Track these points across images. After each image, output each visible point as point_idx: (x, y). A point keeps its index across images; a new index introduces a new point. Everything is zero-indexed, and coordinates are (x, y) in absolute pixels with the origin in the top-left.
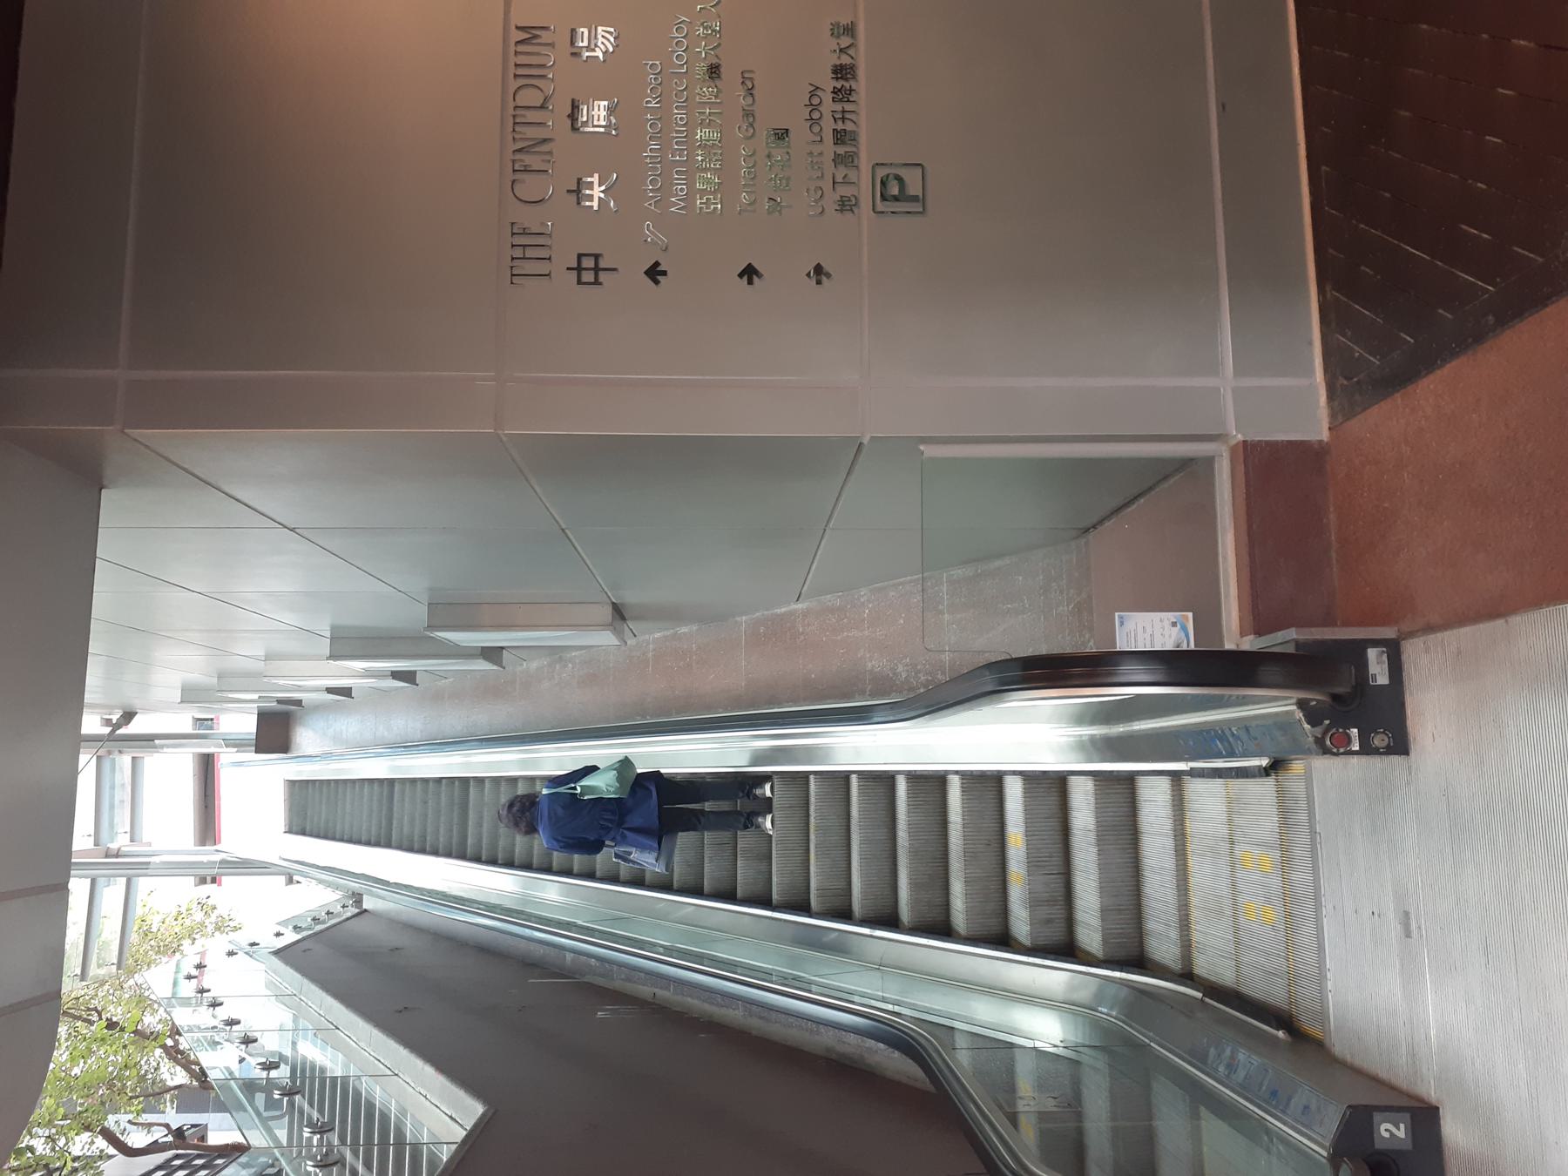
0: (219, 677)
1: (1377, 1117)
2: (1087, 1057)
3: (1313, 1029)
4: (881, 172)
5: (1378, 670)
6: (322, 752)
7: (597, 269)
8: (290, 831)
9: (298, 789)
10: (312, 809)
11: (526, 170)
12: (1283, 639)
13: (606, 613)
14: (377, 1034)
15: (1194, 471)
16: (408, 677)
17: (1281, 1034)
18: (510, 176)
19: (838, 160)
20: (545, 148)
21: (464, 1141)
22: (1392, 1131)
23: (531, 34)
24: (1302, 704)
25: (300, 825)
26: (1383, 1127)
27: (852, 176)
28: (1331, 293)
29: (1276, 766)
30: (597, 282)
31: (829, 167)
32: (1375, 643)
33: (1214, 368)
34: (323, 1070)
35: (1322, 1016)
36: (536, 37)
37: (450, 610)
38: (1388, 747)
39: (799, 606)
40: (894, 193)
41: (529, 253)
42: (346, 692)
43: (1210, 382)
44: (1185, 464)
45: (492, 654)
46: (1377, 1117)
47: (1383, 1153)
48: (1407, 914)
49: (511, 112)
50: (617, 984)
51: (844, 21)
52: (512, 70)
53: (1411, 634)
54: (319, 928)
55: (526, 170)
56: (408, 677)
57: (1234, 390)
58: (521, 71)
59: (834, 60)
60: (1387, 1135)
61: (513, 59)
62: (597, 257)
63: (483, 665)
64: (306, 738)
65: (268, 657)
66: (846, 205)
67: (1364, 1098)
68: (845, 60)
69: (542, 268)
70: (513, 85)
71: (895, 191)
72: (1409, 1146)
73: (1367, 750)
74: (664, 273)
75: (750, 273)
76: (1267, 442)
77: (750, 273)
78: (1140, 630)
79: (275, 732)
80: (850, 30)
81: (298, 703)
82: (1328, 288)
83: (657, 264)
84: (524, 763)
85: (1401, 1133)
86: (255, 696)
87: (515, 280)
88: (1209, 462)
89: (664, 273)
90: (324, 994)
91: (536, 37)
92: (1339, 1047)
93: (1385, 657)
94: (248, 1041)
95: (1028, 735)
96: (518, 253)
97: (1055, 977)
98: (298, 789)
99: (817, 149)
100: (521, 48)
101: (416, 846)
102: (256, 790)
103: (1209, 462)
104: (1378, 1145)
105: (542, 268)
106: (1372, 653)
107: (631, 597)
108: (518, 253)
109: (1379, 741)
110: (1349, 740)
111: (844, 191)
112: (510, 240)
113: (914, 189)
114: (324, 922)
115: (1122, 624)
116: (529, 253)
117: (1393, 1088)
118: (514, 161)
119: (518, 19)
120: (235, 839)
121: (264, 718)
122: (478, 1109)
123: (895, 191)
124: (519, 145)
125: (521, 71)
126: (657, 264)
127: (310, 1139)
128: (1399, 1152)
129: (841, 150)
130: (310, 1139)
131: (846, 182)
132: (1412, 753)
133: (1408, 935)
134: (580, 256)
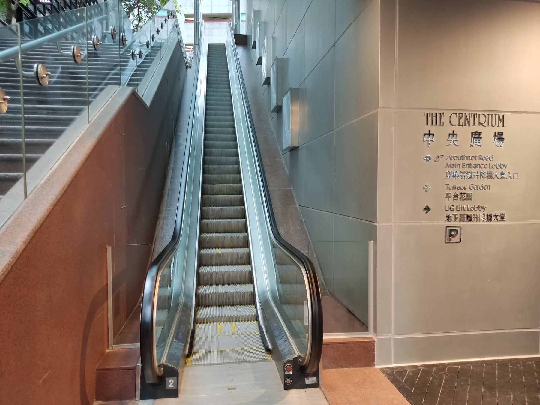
0: (265, 23)
4: (458, 229)
5: (310, 380)
6: (235, 57)
8: (209, 45)
10: (216, 52)
11: (460, 118)
13: (296, 145)
15: (365, 327)
18: (458, 112)
19: (462, 216)
22: (171, 383)
23: (501, 119)
25: (211, 47)
26: (172, 380)
27: (458, 220)
28: (422, 368)
29: (268, 351)
31: (460, 213)
32: (318, 380)
33: (397, 332)
36: (501, 121)
38: (287, 383)
39: (298, 206)
40: (452, 232)
41: (434, 119)
43: (393, 331)
46: (175, 378)
47: (165, 380)
48: (235, 389)
49: (478, 113)
50: (174, 149)
51: (505, 218)
52: (491, 113)
55: (460, 118)
57: (391, 338)
58: (490, 116)
59: (493, 214)
60: (170, 381)
61: (491, 113)
64: (240, 51)
65: (274, 38)
66: (448, 218)
68: (493, 218)
70: (486, 113)
71: (453, 233)
72: (166, 388)
73: (286, 377)
76: (374, 348)
79: (241, 40)
80: (502, 220)
82: (423, 368)
84: (238, 120)
85: (171, 386)
90: (170, 56)
91: (501, 121)
93: (314, 383)
94: (158, 31)
95: (264, 277)
96: (434, 115)
97: (192, 283)
99: (466, 209)
100: (497, 116)
101: (228, 82)
102: (220, 34)
104: (167, 378)
106: (315, 379)
107: (303, 155)
108: (434, 115)
109: (289, 381)
111: (453, 218)
112: (439, 112)
113: (453, 240)
116: (434, 119)
118: (462, 114)
119: (506, 114)
120: (206, 26)
123: (453, 233)
124: (468, 116)
125: (490, 116)
128: (165, 387)
129: (465, 217)
131: (456, 218)
132: (285, 391)
133: (229, 389)
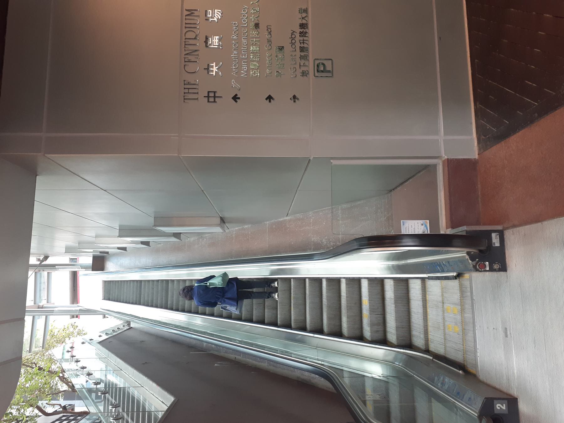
0: (79, 244)
1: (495, 402)
2: (391, 380)
3: (472, 370)
4: (317, 62)
5: (496, 241)
6: (116, 270)
7: (215, 97)
8: (104, 299)
9: (107, 284)
10: (112, 291)
11: (189, 61)
12: (462, 230)
13: (218, 220)
14: (135, 372)
15: (430, 169)
16: (147, 243)
17: (461, 372)
18: (184, 63)
19: (301, 57)
20: (196, 53)
21: (167, 410)
22: (501, 407)
23: (191, 12)
24: (468, 253)
25: (108, 297)
26: (498, 405)
27: (307, 63)
28: (479, 105)
29: (459, 276)
30: (215, 102)
31: (298, 60)
32: (495, 231)
33: (437, 132)
34: (116, 385)
35: (476, 365)
36: (193, 13)
37: (162, 219)
38: (499, 269)
39: (288, 218)
40: (322, 69)
41: (190, 91)
42: (124, 249)
43: (435, 137)
44: (426, 167)
45: (177, 235)
46: (495, 402)
47: (497, 415)
48: (506, 329)
49: (184, 40)
50: (222, 354)
51: (304, 8)
52: (184, 25)
53: (508, 228)
54: (115, 334)
55: (189, 61)
56: (147, 243)
57: (444, 140)
58: (187, 26)
59: (300, 22)
60: (499, 408)
61: (184, 21)
62: (215, 92)
63: (174, 239)
64: (110, 265)
65: (97, 236)
66: (304, 74)
67: (491, 395)
68: (304, 22)
69: (195, 96)
70: (185, 30)
71: (322, 69)
72: (507, 412)
73: (492, 270)
74: (239, 98)
75: (270, 98)
76: (456, 159)
77: (270, 98)
78: (410, 227)
79: (99, 263)
80: (306, 11)
81: (107, 253)
82: (478, 104)
83: (236, 95)
84: (188, 275)
85: (504, 407)
86: (92, 250)
87: (185, 101)
88: (435, 166)
89: (239, 98)
90: (116, 358)
91: (193, 13)
92: (481, 377)
93: (498, 236)
94: (89, 374)
95: (370, 264)
96: (186, 91)
97: (379, 351)
98: (107, 284)
99: (294, 54)
100: (187, 17)
101: (150, 304)
102: (92, 284)
103: (435, 166)
104: (496, 412)
105: (195, 96)
106: (493, 235)
107: (227, 215)
108: (186, 91)
109: (496, 266)
110: (485, 266)
111: (304, 69)
112: (183, 86)
113: (329, 68)
114: (116, 332)
115: (403, 224)
116: (190, 91)
117: (501, 391)
118: (185, 58)
119: (186, 7)
120: (84, 302)
121: (95, 258)
122: (172, 399)
123: (322, 69)
124: (187, 52)
125: (187, 26)
126: (236, 95)
127: (111, 410)
128: (503, 415)
129: (303, 54)
130: (111, 410)
131: (304, 65)
132: (508, 271)
133: (506, 336)
134: (209, 92)
